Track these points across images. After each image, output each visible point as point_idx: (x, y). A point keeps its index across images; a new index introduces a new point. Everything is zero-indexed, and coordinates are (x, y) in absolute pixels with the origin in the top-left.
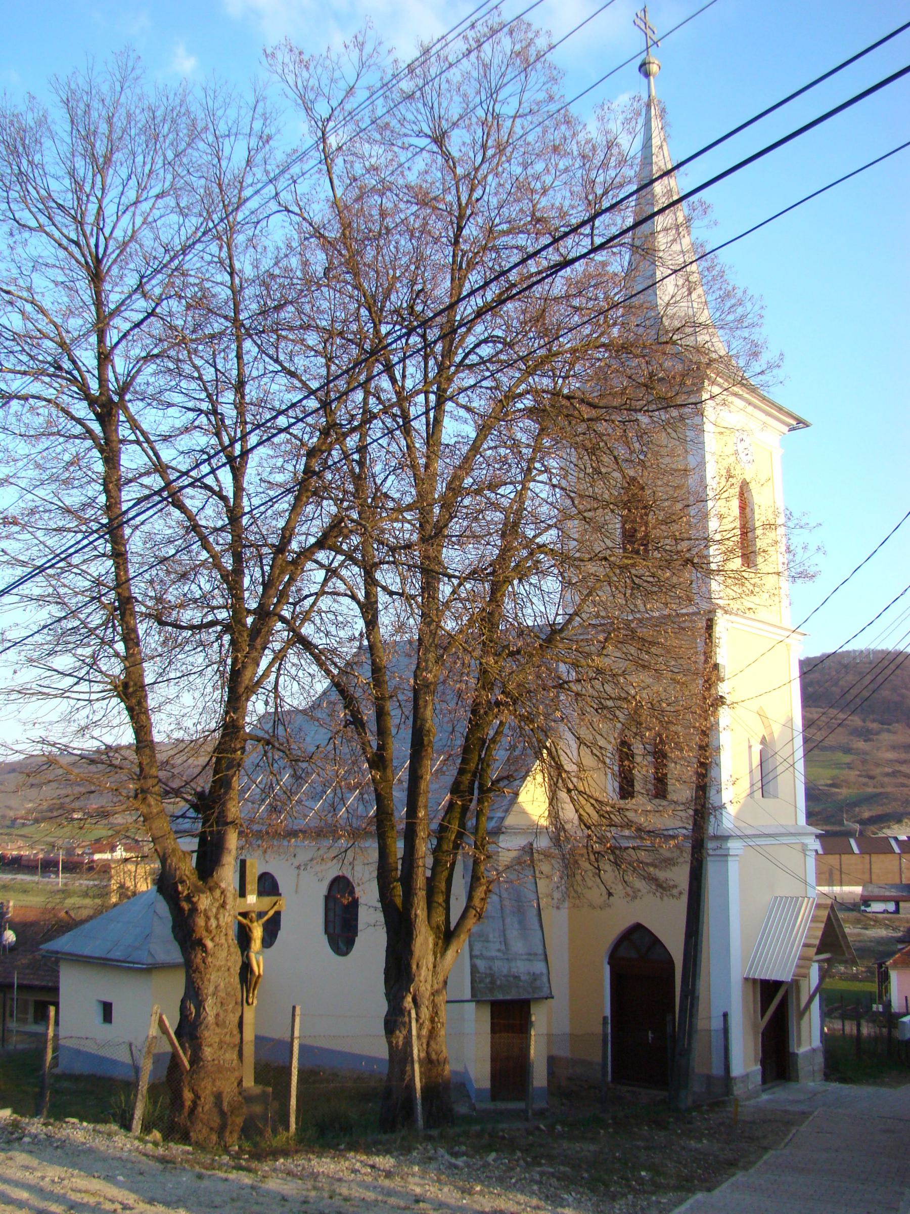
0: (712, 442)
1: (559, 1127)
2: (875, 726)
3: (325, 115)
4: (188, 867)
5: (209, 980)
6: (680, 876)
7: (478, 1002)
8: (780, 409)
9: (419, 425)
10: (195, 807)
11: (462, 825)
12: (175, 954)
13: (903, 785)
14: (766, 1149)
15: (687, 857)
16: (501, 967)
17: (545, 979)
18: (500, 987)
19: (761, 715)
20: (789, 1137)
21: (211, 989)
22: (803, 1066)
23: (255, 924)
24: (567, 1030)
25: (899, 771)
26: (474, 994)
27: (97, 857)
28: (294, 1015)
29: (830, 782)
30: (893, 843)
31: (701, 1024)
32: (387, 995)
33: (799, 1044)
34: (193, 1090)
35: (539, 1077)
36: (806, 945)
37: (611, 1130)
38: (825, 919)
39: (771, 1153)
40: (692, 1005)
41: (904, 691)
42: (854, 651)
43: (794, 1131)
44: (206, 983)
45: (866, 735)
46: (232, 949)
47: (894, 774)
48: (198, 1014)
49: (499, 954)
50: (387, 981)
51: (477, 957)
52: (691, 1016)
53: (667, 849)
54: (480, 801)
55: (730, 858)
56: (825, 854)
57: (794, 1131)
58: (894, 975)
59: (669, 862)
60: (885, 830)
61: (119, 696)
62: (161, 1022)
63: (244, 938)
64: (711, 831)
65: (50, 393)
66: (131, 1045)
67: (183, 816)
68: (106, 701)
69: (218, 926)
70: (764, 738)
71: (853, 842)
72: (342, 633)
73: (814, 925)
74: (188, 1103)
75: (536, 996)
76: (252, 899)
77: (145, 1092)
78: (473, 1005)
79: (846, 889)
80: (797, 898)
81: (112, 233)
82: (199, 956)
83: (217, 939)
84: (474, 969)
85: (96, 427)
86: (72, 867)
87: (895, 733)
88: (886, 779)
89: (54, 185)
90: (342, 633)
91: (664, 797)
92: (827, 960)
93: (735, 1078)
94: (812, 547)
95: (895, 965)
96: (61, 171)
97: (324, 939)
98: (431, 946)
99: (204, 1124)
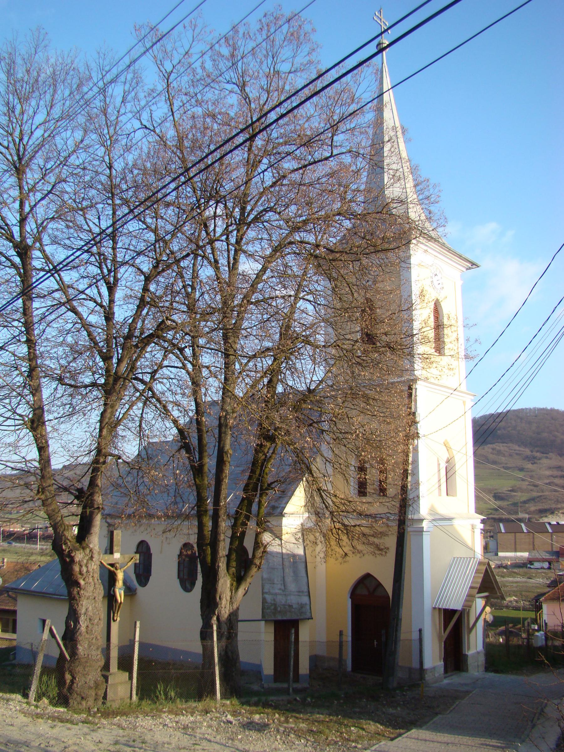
1: (309, 699)
2: (538, 455)
3: (169, 70)
5: (82, 605)
6: (391, 542)
7: (266, 621)
8: (460, 257)
9: (223, 261)
10: (77, 497)
11: (249, 511)
12: (63, 588)
13: (555, 491)
14: (437, 714)
16: (280, 599)
17: (308, 607)
18: (280, 612)
21: (83, 611)
23: (119, 571)
24: (324, 639)
25: (553, 483)
26: (263, 616)
28: (135, 627)
29: (510, 489)
31: (403, 636)
32: (202, 615)
33: (469, 648)
35: (304, 667)
36: (471, 588)
37: (342, 701)
38: (484, 571)
39: (440, 716)
40: (397, 625)
41: (556, 433)
42: (526, 409)
43: (457, 703)
45: (532, 460)
46: (97, 586)
47: (549, 484)
48: (75, 626)
49: (280, 591)
51: (266, 593)
53: (379, 526)
54: (261, 495)
58: (545, 606)
59: (383, 534)
62: (51, 631)
67: (71, 503)
69: (88, 571)
74: (68, 681)
75: (302, 617)
76: (117, 555)
79: (519, 554)
84: (264, 601)
85: (17, 260)
87: (551, 459)
93: (427, 670)
94: (472, 340)
95: (546, 600)
97: (177, 582)
98: (229, 585)
99: (77, 694)
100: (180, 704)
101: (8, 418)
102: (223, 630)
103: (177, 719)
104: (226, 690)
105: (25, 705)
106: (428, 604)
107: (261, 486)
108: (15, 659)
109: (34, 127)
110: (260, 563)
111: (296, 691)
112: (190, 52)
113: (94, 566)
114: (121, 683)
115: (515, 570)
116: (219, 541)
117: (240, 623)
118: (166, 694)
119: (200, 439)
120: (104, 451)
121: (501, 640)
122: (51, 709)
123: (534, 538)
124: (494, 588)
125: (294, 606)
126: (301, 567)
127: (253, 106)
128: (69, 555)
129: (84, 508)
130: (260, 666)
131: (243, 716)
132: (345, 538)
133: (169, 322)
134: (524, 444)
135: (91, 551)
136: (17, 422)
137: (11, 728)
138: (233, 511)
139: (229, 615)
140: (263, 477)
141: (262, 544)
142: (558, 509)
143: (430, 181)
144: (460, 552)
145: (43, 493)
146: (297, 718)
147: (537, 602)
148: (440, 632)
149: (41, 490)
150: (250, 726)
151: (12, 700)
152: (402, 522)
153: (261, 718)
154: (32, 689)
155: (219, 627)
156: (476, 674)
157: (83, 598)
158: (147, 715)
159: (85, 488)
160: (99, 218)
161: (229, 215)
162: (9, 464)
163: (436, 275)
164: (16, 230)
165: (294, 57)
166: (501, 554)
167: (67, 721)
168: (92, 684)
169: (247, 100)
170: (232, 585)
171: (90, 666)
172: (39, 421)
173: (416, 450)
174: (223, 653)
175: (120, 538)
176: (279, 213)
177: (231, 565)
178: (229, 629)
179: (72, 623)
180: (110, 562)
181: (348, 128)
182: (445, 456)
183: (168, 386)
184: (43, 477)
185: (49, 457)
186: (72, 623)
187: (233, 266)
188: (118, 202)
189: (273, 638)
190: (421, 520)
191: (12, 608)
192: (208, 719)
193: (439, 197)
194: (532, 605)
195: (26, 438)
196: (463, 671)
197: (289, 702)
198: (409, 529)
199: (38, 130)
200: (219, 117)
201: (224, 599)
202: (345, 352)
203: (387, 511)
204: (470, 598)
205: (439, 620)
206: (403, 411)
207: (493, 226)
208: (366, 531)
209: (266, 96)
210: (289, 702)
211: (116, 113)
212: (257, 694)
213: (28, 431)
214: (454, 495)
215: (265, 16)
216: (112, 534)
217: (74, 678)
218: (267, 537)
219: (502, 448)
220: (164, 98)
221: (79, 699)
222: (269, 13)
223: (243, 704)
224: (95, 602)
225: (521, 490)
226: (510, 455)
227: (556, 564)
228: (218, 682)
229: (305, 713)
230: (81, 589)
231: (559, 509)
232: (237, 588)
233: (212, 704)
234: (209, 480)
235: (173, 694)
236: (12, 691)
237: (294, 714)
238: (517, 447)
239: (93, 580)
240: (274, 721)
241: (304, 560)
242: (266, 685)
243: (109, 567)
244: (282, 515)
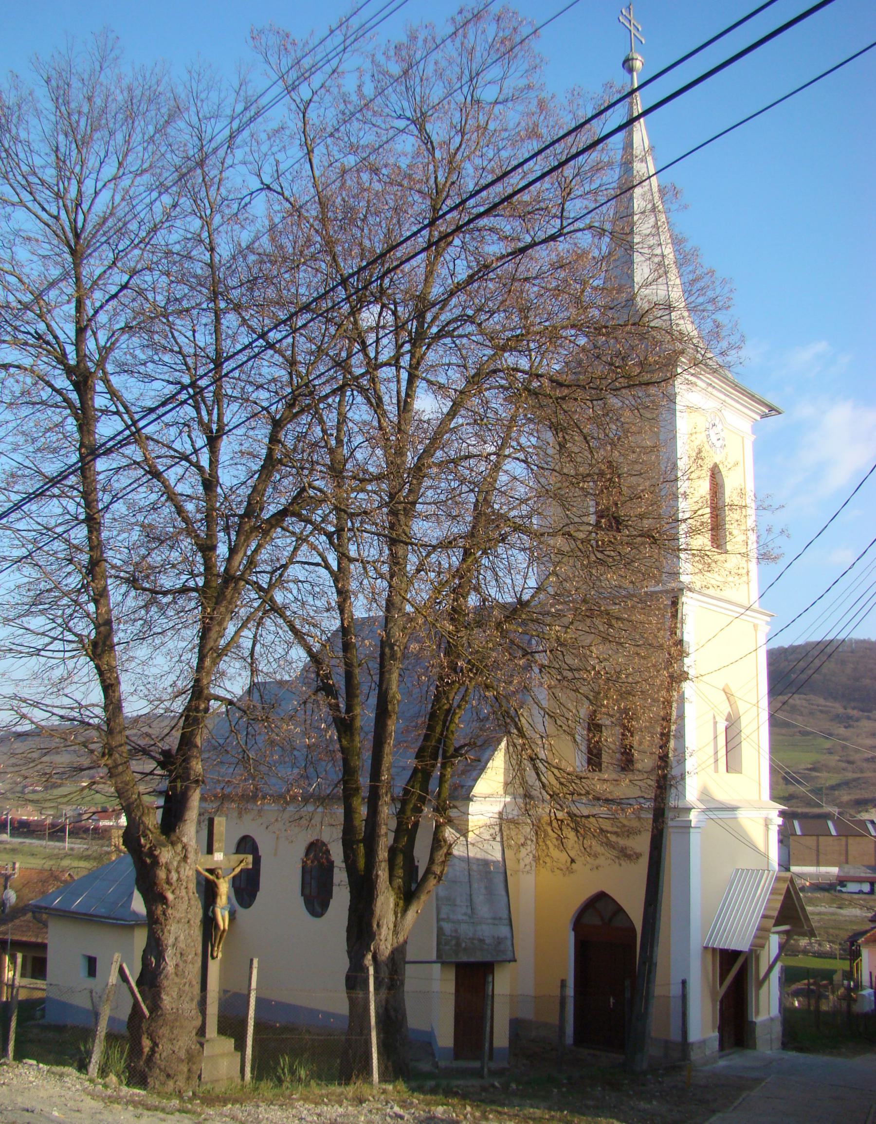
0: (684, 423)
1: (514, 1086)
2: (855, 713)
4: (154, 819)
5: (169, 932)
6: (642, 843)
7: (443, 963)
10: (162, 765)
11: (425, 788)
14: (714, 1112)
15: (649, 825)
16: (466, 930)
17: (509, 942)
19: (728, 694)
21: (171, 941)
23: (221, 880)
28: (251, 967)
29: (810, 766)
30: (870, 826)
31: (658, 990)
32: (349, 952)
33: (757, 1013)
34: (152, 1039)
35: (501, 1037)
36: (764, 917)
37: (564, 1089)
38: (784, 892)
40: (650, 972)
44: (166, 933)
45: (846, 721)
46: (192, 902)
49: (464, 918)
50: (349, 939)
51: (443, 920)
52: (648, 983)
53: (627, 817)
54: (444, 766)
55: (692, 830)
56: (803, 835)
58: (865, 952)
59: (629, 832)
61: (87, 655)
62: (121, 971)
63: (208, 892)
64: (672, 803)
65: (27, 362)
66: (91, 992)
67: (151, 773)
68: (75, 660)
69: (179, 879)
70: (729, 714)
71: (830, 824)
72: (318, 603)
74: (146, 1050)
75: (499, 959)
76: (219, 856)
77: (103, 1038)
78: (437, 967)
79: (823, 869)
81: (90, 208)
83: (177, 892)
84: (440, 931)
85: (74, 396)
86: (79, 831)
88: (865, 765)
89: (38, 162)
90: (318, 603)
92: (786, 932)
93: (692, 1044)
95: (867, 942)
96: (45, 149)
97: (301, 900)
98: (392, 905)
100: (316, 1089)
101: (55, 639)
102: (382, 975)
103: (318, 1111)
104: (386, 1067)
105: (87, 1083)
106: (696, 942)
107: (445, 752)
108: (43, 1016)
109: (100, 185)
110: (442, 872)
111: (493, 1073)
112: (340, 70)
113: (188, 872)
114: (223, 1055)
115: (818, 895)
117: (407, 966)
118: (292, 1072)
119: (349, 676)
120: (206, 692)
121: (796, 1004)
122: (125, 1090)
123: (847, 845)
124: (799, 919)
126: (499, 880)
127: (438, 154)
128: (151, 854)
129: (173, 781)
130: (431, 1034)
131: (416, 1107)
132: (571, 835)
133: (311, 492)
134: (831, 695)
135: (184, 847)
137: (77, 1114)
138: (398, 792)
139: (393, 952)
140: (446, 736)
141: (445, 841)
143: (716, 275)
144: (747, 862)
145: (110, 755)
146: (500, 1113)
147: (852, 944)
149: (110, 750)
151: (68, 1075)
152: (660, 814)
153: (445, 1112)
154: (93, 1060)
155: (376, 971)
156: (769, 1052)
157: (170, 921)
158: (272, 1103)
159: (174, 751)
160: (194, 331)
161: (398, 328)
162: (56, 710)
163: (714, 425)
164: (70, 350)
165: (503, 78)
166: (794, 869)
167: (156, 1108)
168: (183, 1054)
169: (429, 146)
170: (397, 905)
171: (181, 1027)
172: (104, 644)
173: (682, 699)
174: (381, 1011)
175: (223, 829)
176: (480, 325)
177: (395, 873)
178: (390, 974)
179: (153, 960)
180: (208, 867)
181: (587, 189)
182: (726, 709)
183: (295, 592)
184: (110, 732)
185: (120, 701)
186: (153, 960)
187: (405, 405)
188: (223, 305)
190: (688, 810)
191: (40, 940)
192: (365, 1111)
193: (730, 299)
194: (844, 950)
195: (85, 670)
197: (484, 1089)
198: (671, 823)
199: (104, 191)
200: (384, 171)
201: (385, 927)
202: (579, 543)
203: (639, 794)
204: (762, 933)
205: (712, 966)
206: (663, 638)
207: (821, 347)
208: (607, 825)
209: (458, 139)
210: (484, 1089)
211: (219, 165)
212: (430, 1076)
213: (88, 659)
214: (739, 771)
215: (460, 12)
216: (211, 822)
217: (155, 1044)
218: (449, 833)
219: (798, 702)
220: (298, 142)
221: (162, 1077)
223: (413, 1090)
224: (190, 927)
225: (828, 769)
226: (811, 713)
228: (375, 1055)
229: (511, 1105)
230: (168, 906)
232: (405, 910)
233: (365, 1090)
234: (364, 743)
235: (303, 1073)
236: (63, 1064)
237: (494, 1107)
238: (821, 701)
239: (187, 893)
240: (465, 1117)
241: (502, 870)
242: (442, 1064)
243: (207, 874)
244: (468, 798)
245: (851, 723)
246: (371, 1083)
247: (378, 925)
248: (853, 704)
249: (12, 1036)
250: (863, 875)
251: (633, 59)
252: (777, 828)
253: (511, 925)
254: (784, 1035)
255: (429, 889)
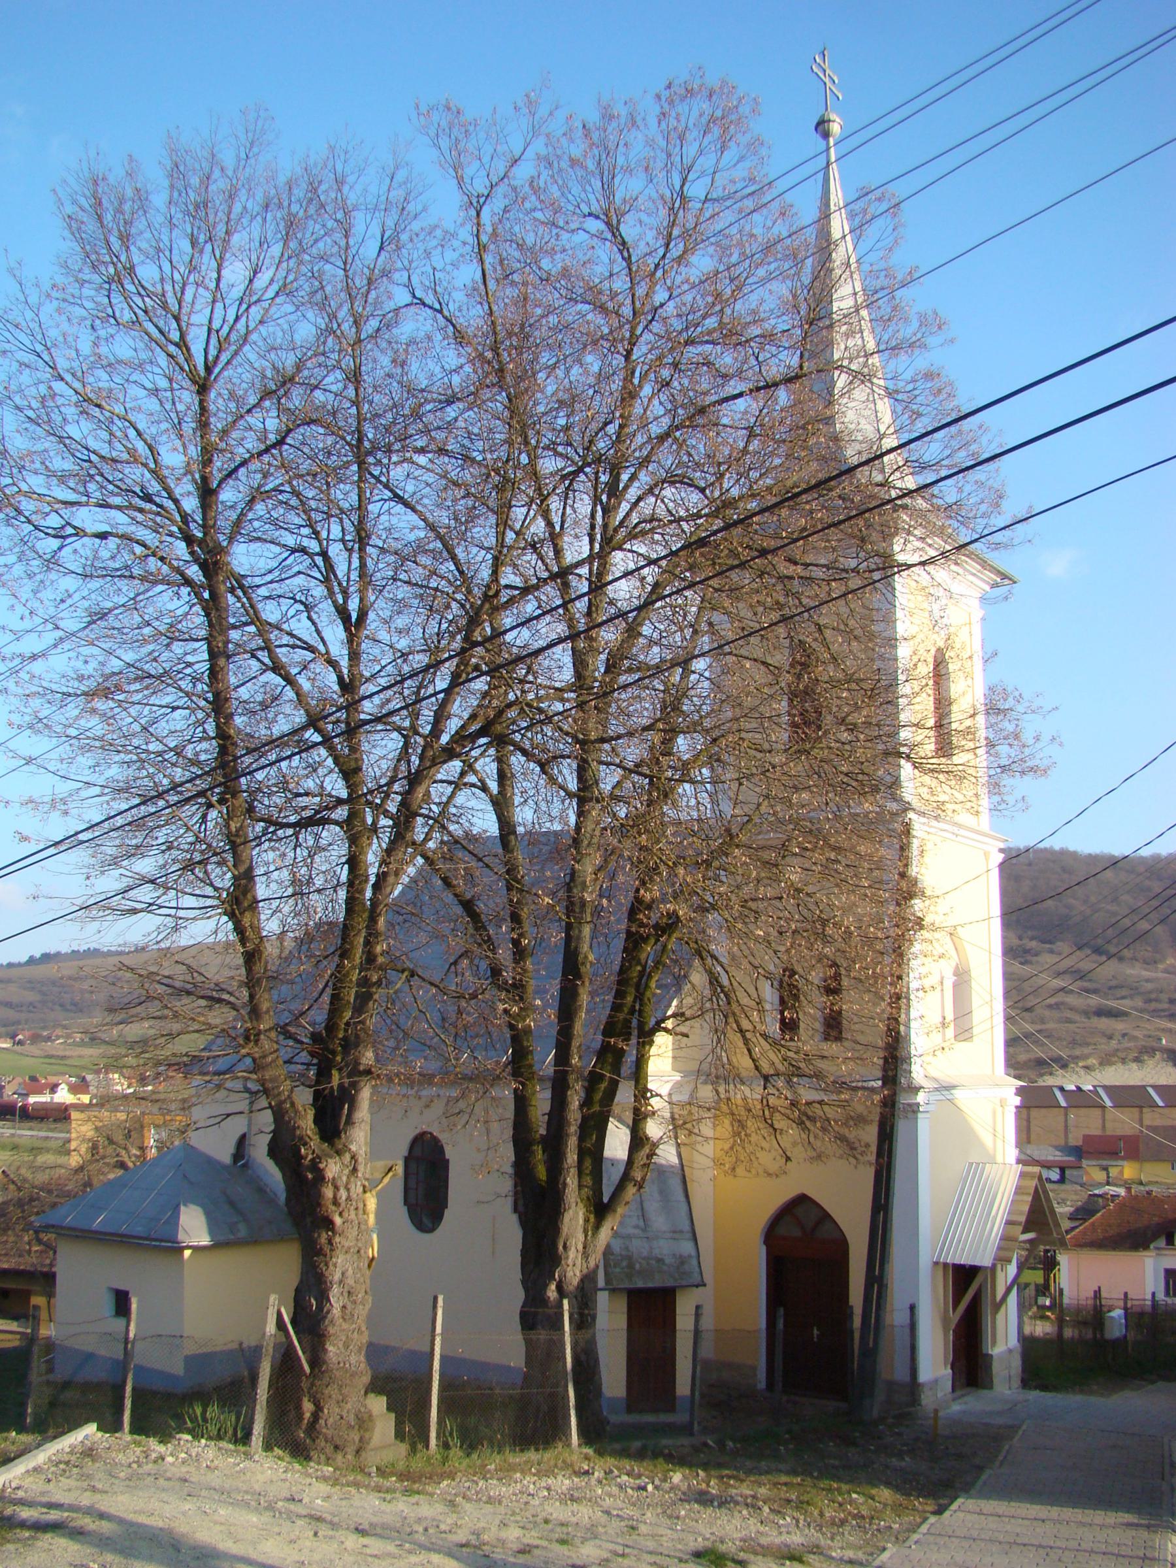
1: (730, 1444)
5: (335, 1265)
6: (870, 1134)
14: (980, 1469)
16: (639, 1247)
17: (694, 1262)
20: (1001, 1458)
21: (337, 1276)
22: (999, 1371)
23: (368, 1195)
25: (1063, 1003)
27: (32, 1099)
28: (435, 1307)
30: (1058, 1094)
32: (524, 1282)
36: (1008, 1223)
38: (1032, 1191)
43: (1007, 1447)
44: (331, 1267)
48: (320, 1307)
55: (920, 1115)
57: (1007, 1447)
59: (860, 1120)
60: (1045, 1078)
69: (349, 1199)
73: (1019, 1198)
74: (307, 1415)
75: (684, 1283)
80: (978, 1164)
82: (324, 1235)
83: (345, 1214)
85: (194, 572)
88: (1047, 1013)
91: (839, 1039)
97: (404, 1211)
98: (581, 1221)
106: (925, 1258)
110: (643, 1179)
116: (568, 1135)
125: (667, 1261)
136: (209, 902)
139: (582, 1280)
142: (1076, 1059)
148: (946, 1311)
150: (704, 1499)
156: (1008, 1392)
157: (338, 1252)
169: (626, 254)
170: (587, 1220)
189: (625, 1327)
190: (917, 1089)
196: (984, 1387)
197: (696, 1450)
201: (573, 1249)
215: (669, 87)
217: (319, 1408)
221: (329, 1449)
222: (676, 82)
227: (1075, 1172)
231: (1077, 1057)
232: (597, 1227)
245: (1029, 958)
246: (569, 1445)
247: (565, 1247)
248: (1030, 933)
249: (128, 1403)
250: (1051, 1158)
251: (829, 121)
252: (1014, 1110)
253: (695, 1239)
254: (1024, 1371)
255: (627, 1199)
